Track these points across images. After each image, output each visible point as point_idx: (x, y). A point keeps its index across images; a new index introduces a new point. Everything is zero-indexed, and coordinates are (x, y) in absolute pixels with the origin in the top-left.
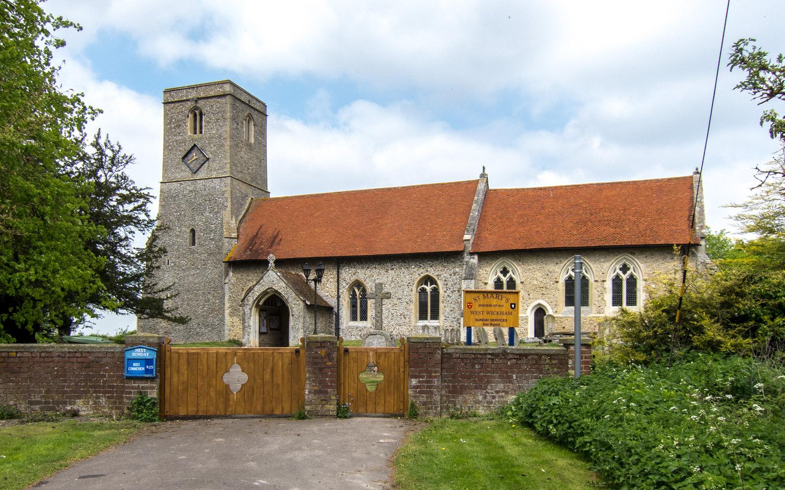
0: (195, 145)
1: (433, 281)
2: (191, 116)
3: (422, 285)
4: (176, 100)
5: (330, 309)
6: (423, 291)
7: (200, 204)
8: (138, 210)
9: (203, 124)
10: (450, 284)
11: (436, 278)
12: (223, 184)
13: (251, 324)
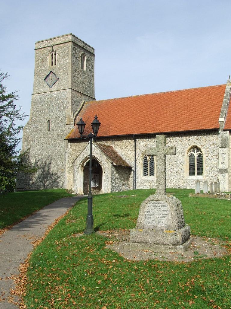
0: (51, 71)
1: (198, 149)
2: (50, 55)
3: (191, 152)
4: (42, 47)
5: (129, 169)
6: (192, 156)
7: (53, 106)
8: (8, 106)
9: (56, 59)
10: (210, 151)
11: (200, 147)
12: (66, 94)
13: (78, 178)
